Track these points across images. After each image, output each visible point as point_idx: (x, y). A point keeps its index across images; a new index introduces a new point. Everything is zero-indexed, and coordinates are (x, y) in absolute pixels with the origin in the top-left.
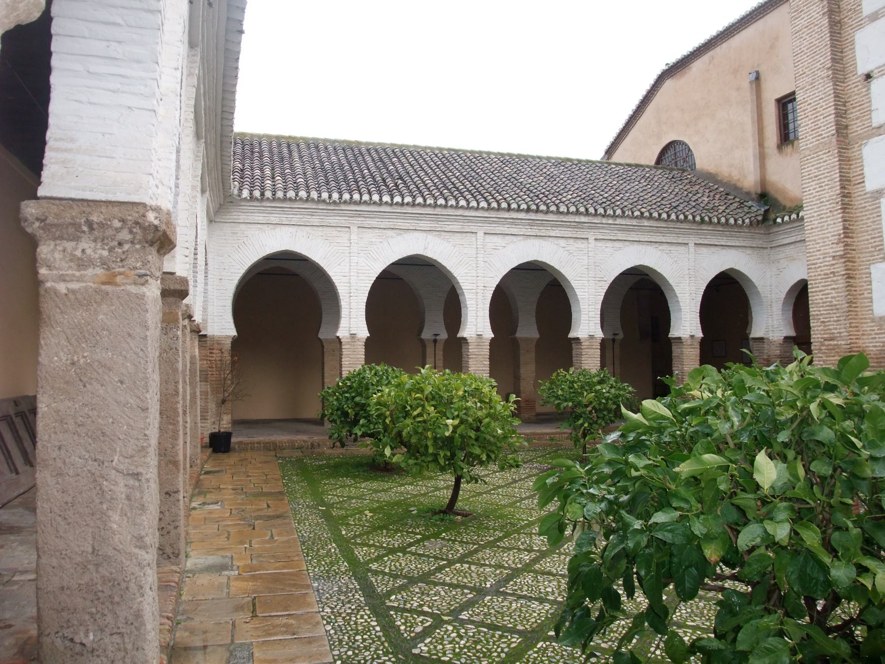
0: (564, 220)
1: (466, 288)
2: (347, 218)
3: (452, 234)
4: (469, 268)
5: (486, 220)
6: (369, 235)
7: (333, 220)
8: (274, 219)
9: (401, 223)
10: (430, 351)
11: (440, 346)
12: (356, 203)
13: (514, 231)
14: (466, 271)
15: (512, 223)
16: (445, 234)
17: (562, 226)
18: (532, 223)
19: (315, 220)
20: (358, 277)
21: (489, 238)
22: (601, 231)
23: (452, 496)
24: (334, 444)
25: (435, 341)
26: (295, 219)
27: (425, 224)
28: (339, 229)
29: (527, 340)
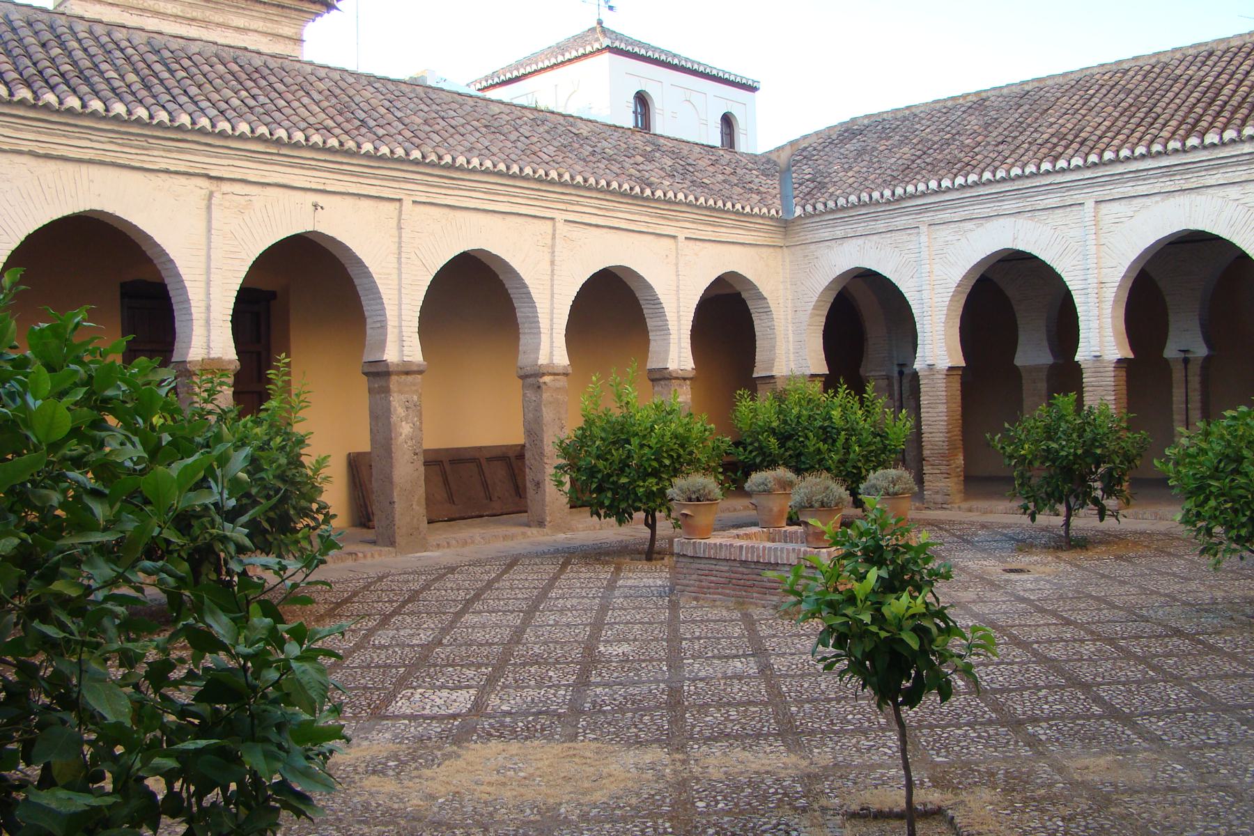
0: (1222, 155)
1: (1075, 287)
2: (914, 216)
3: (1050, 211)
4: (1078, 258)
5: (1091, 183)
6: (944, 233)
7: (901, 222)
8: (839, 232)
11: (1195, 369)
14: (1075, 262)
15: (1137, 179)
16: (1040, 213)
19: (880, 226)
20: (933, 289)
21: (1105, 208)
24: (13, 504)
25: (1186, 361)
26: (861, 228)
27: (1010, 206)
28: (909, 231)
29: (1037, 369)
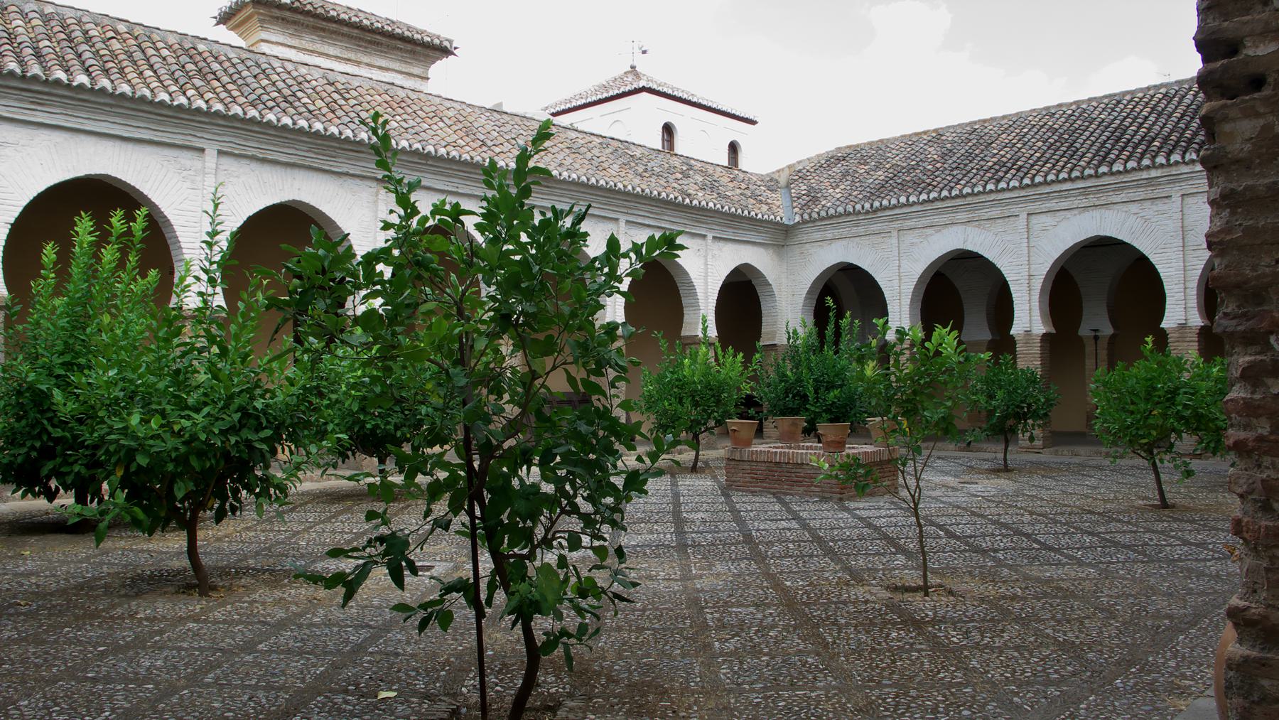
8: (829, 235)
9: (937, 219)
10: (1089, 348)
11: (1103, 344)
12: (904, 205)
13: (1064, 205)
14: (1010, 260)
15: (1060, 197)
17: (1128, 187)
18: (1084, 192)
19: (861, 230)
22: (1191, 182)
23: (189, 547)
27: (962, 216)
